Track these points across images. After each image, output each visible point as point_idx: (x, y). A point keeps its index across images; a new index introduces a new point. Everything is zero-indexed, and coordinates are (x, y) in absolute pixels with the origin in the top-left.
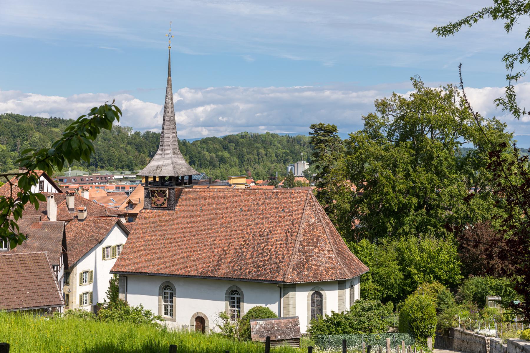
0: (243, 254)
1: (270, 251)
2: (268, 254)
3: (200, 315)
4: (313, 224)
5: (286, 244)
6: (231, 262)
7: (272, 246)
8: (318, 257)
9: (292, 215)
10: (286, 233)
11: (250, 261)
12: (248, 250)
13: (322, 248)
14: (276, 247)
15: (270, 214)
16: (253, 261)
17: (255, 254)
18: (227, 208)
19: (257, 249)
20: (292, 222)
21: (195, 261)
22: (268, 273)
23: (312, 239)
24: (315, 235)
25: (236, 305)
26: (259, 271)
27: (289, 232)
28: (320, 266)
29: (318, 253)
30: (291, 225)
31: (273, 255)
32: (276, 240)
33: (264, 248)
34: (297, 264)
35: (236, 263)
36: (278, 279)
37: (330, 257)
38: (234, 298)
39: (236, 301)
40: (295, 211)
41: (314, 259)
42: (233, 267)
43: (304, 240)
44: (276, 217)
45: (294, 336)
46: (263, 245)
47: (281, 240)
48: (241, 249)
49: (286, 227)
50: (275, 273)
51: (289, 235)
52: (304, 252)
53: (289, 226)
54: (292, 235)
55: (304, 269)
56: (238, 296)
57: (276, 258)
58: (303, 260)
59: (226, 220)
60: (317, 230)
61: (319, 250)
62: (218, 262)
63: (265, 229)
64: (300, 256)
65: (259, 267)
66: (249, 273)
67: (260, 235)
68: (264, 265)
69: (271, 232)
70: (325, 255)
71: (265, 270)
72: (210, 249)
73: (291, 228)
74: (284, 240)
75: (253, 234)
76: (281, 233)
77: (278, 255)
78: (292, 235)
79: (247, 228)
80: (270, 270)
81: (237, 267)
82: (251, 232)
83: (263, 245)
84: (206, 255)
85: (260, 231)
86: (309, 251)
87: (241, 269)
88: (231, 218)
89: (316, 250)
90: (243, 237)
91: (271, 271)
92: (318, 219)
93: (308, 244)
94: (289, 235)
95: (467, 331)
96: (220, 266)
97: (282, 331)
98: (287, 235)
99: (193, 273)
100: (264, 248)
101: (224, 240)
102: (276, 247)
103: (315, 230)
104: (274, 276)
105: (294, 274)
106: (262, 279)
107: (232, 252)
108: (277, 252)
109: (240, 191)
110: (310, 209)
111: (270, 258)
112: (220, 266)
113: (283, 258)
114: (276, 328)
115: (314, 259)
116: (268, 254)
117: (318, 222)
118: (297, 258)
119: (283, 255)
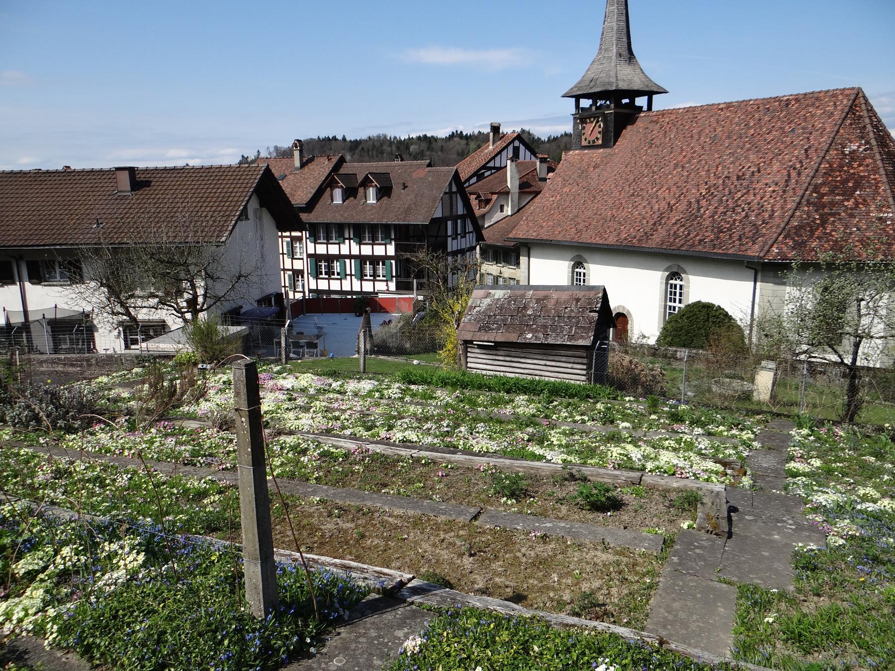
0: (699, 210)
1: (749, 204)
2: (743, 210)
3: (621, 311)
4: (853, 152)
5: (784, 191)
6: (675, 223)
7: (755, 195)
8: (852, 216)
9: (808, 138)
10: (789, 171)
11: (707, 223)
12: (710, 204)
13: (865, 200)
14: (762, 198)
15: (765, 140)
16: (714, 221)
17: (721, 209)
18: (692, 136)
19: (727, 201)
20: (806, 150)
21: (620, 223)
22: (734, 242)
23: (846, 181)
24: (854, 174)
25: (678, 297)
26: (718, 238)
27: (795, 169)
28: (851, 234)
29: (851, 209)
30: (802, 157)
31: (753, 211)
32: (767, 184)
33: (739, 199)
34: (801, 227)
35: (683, 226)
36: (750, 253)
37: (880, 219)
38: (676, 286)
39: (678, 291)
40: (817, 130)
41: (840, 219)
42: (675, 232)
43: (824, 184)
44: (776, 144)
45: (571, 337)
46: (739, 194)
47: (776, 184)
48: (698, 202)
49: (790, 161)
50: (747, 243)
51: (794, 174)
52: (819, 206)
53: (797, 157)
54: (799, 174)
55: (811, 236)
56: (681, 283)
57: (756, 216)
58: (814, 221)
59: (685, 157)
60: (860, 165)
61: (857, 204)
62: (654, 224)
63: (749, 167)
64: (808, 213)
65: (721, 232)
66: (700, 241)
67: (738, 178)
68: (729, 229)
69: (759, 171)
70: (868, 213)
71: (731, 238)
72: (649, 203)
73: (801, 162)
74: (782, 184)
75: (726, 177)
76: (779, 171)
77: (763, 211)
78: (799, 174)
79: (717, 167)
80: (740, 236)
81: (683, 232)
82: (723, 173)
83: (739, 194)
84: (639, 214)
85: (740, 170)
86: (832, 204)
87: (689, 234)
88: (694, 152)
89: (850, 203)
90: (706, 183)
91: (740, 239)
92: (867, 143)
93: (832, 192)
94: (794, 174)
95: (283, 344)
96: (656, 230)
97: (541, 321)
98: (789, 175)
99: (612, 240)
100: (739, 199)
101: (674, 189)
102: (762, 198)
103: (855, 165)
104: (743, 248)
105: (786, 244)
106: (721, 251)
107: (682, 206)
108: (763, 206)
109: (721, 106)
110: (851, 124)
111: (747, 216)
112: (656, 230)
113: (771, 217)
114: (529, 312)
115: (840, 219)
116: (743, 210)
117: (865, 150)
118: (801, 216)
119: (773, 211)
